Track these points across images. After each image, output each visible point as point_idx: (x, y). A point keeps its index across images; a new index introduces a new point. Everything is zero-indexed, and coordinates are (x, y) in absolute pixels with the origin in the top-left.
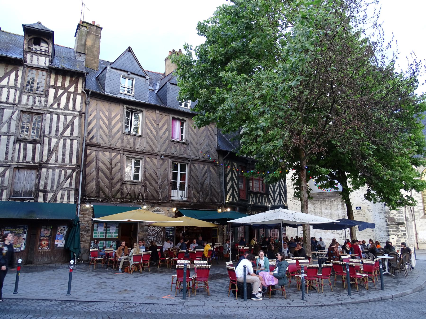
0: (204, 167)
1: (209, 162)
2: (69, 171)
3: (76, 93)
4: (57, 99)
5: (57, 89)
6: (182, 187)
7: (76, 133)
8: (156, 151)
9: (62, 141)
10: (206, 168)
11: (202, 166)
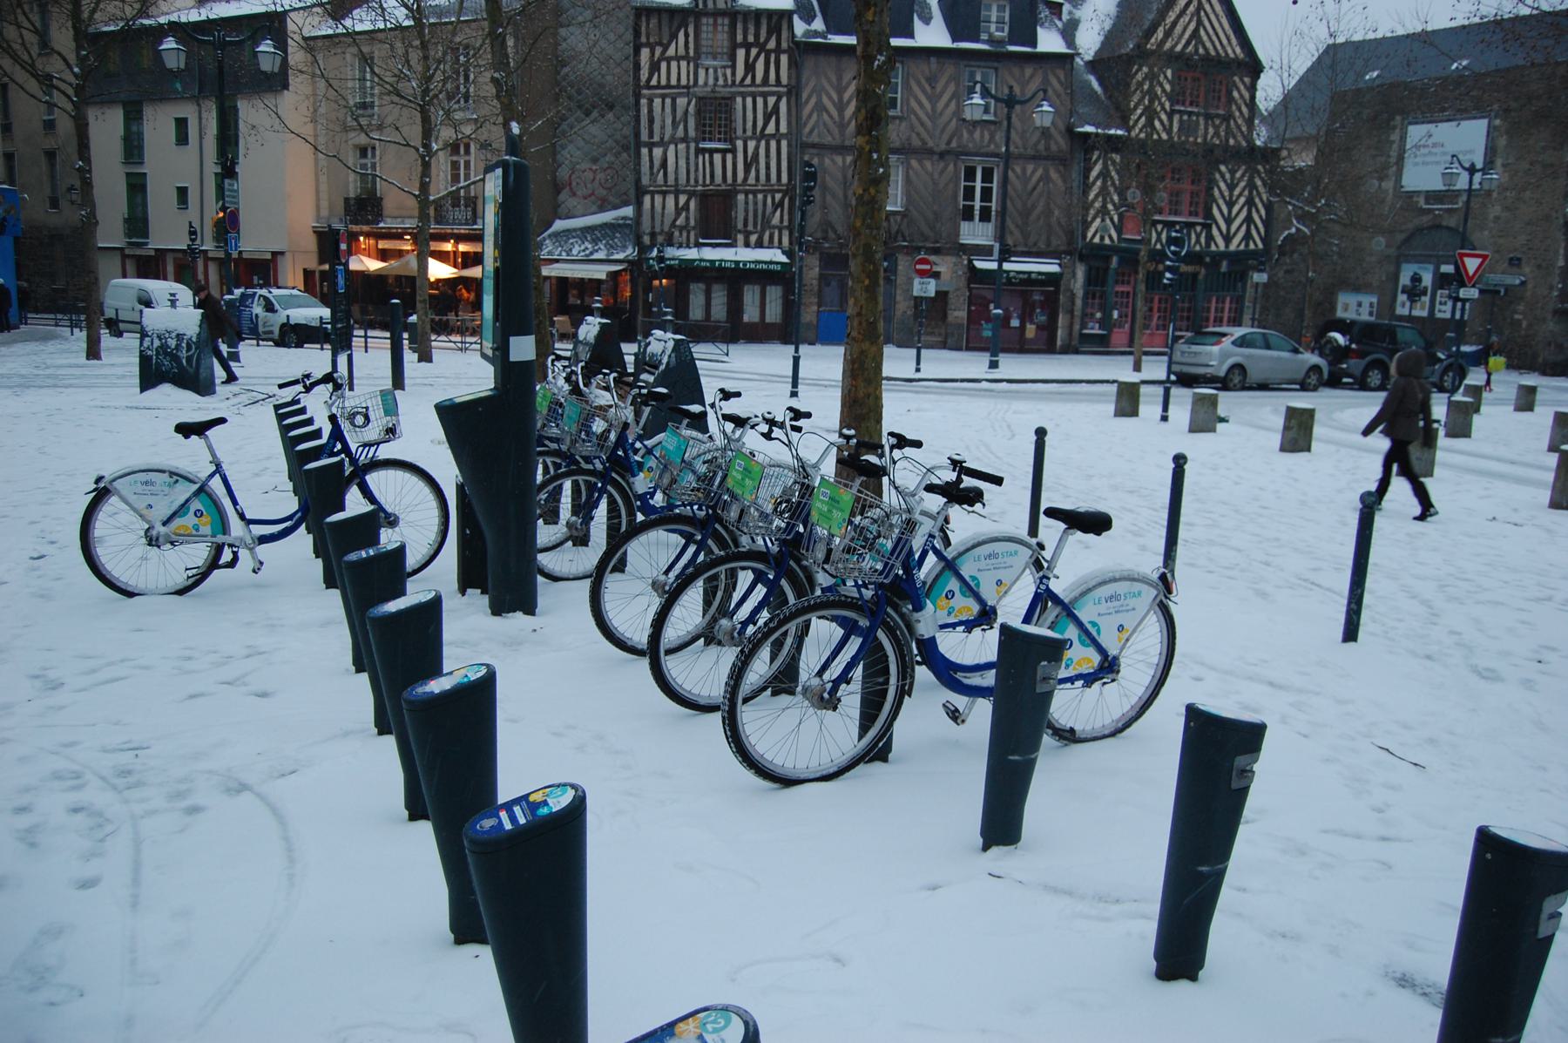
0: (1033, 172)
1: (1046, 158)
2: (778, 196)
3: (778, 50)
4: (750, 68)
5: (748, 47)
6: (985, 216)
7: (783, 129)
8: (931, 144)
9: (763, 143)
10: (1040, 172)
11: (1030, 168)
